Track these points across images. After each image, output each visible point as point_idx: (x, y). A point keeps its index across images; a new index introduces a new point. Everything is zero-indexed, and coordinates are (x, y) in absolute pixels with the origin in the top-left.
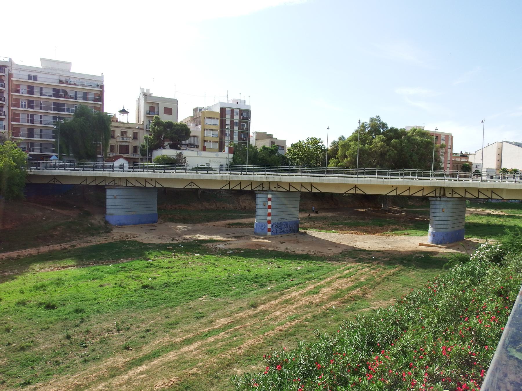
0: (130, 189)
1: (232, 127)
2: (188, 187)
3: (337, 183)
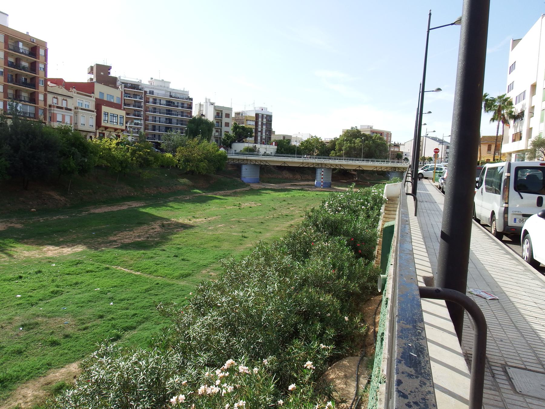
1: (262, 127)
2: (283, 165)
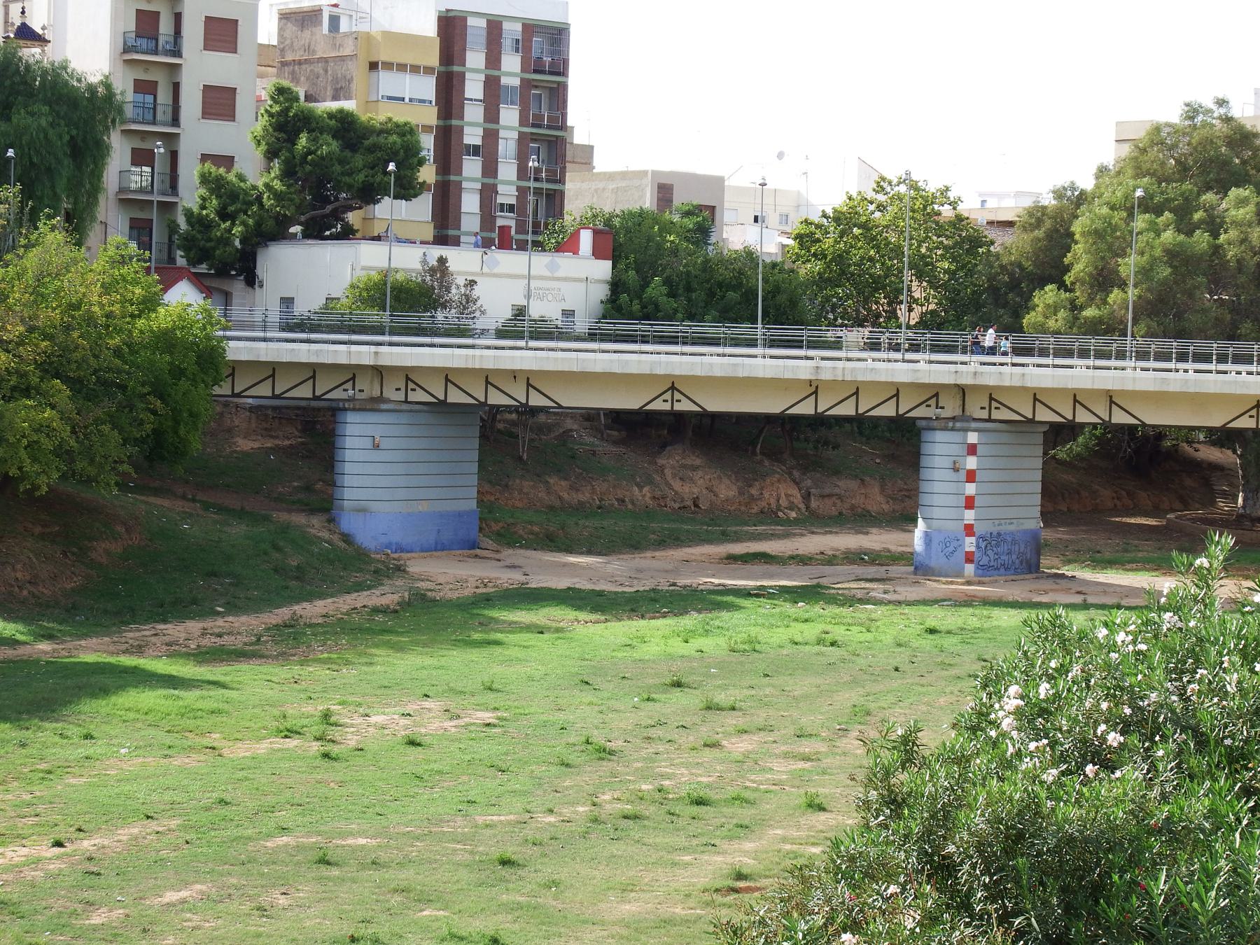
0: (411, 411)
2: (658, 405)
3: (1212, 391)
